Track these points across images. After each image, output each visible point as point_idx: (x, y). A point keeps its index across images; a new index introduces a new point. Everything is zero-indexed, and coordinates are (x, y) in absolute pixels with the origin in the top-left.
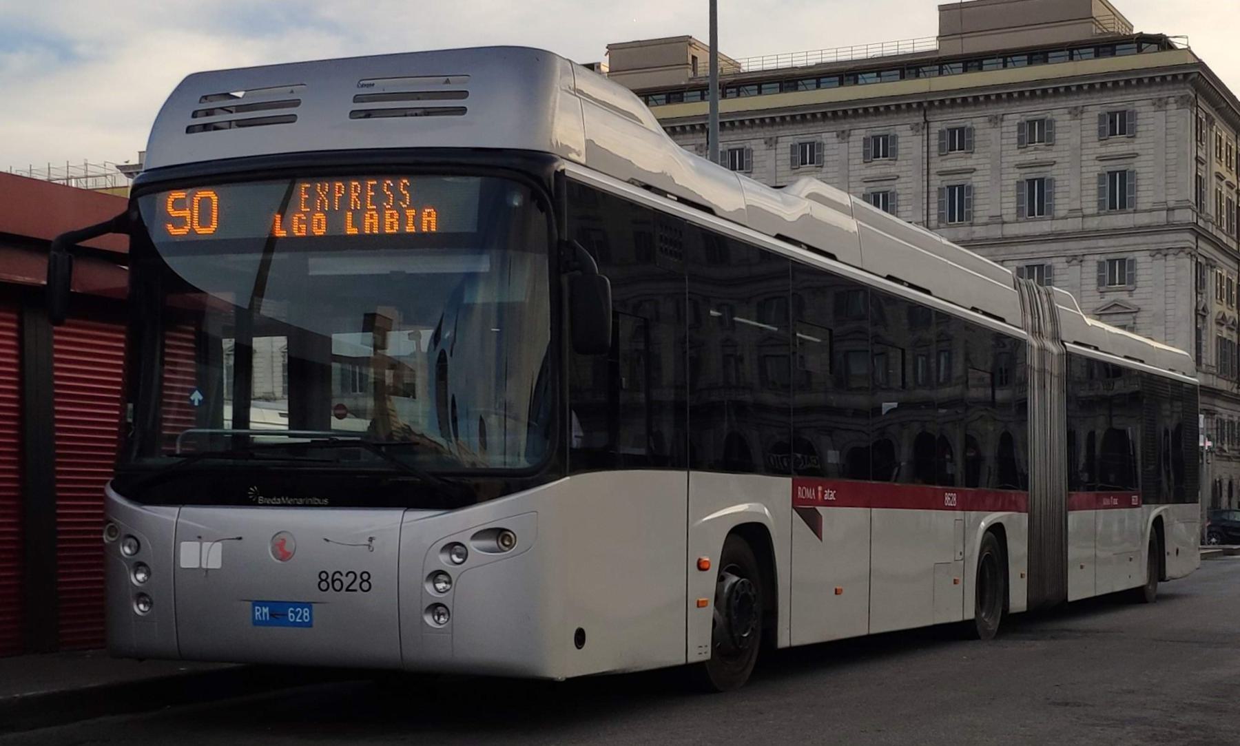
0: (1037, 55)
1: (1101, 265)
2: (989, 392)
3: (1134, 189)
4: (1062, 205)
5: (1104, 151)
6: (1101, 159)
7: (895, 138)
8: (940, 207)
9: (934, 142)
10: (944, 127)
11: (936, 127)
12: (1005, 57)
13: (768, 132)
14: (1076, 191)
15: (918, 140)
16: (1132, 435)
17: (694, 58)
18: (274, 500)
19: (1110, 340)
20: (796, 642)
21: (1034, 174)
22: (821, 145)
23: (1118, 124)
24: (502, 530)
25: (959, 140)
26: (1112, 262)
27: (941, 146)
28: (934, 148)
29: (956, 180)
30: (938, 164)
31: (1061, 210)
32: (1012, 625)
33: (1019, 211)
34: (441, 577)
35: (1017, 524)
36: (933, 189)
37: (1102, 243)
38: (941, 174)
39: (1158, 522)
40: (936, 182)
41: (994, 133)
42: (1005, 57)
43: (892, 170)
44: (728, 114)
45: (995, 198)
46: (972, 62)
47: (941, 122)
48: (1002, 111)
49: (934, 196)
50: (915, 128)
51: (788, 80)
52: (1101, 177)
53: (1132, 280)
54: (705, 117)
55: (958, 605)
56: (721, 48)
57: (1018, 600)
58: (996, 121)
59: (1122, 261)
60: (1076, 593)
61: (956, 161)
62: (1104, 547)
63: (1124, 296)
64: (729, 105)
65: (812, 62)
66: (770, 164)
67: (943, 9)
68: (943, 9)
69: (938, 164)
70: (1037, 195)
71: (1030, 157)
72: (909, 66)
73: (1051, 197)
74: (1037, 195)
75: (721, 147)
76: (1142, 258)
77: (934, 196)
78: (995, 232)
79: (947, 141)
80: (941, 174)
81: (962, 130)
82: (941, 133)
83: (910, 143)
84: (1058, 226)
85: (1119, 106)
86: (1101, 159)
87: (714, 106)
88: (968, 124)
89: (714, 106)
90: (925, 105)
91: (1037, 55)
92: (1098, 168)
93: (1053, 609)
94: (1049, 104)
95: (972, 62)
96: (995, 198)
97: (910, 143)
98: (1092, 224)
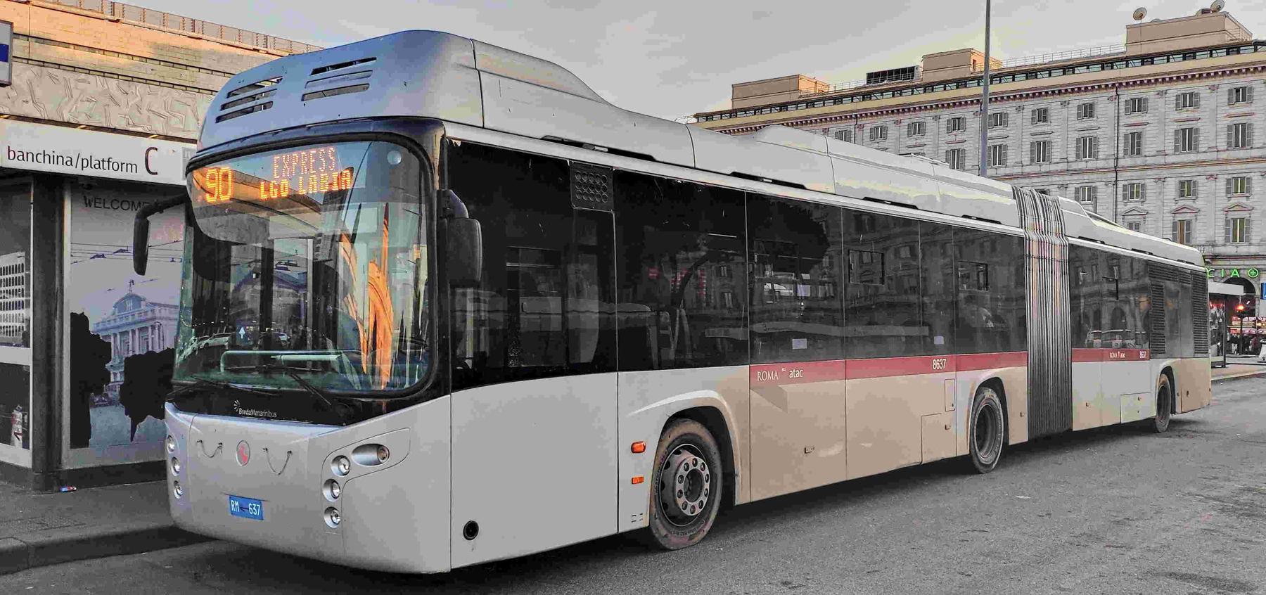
0: (1189, 54)
1: (1228, 181)
2: (570, 307)
3: (1251, 135)
4: (1056, 154)
5: (1232, 111)
9: (1122, 108)
11: (1122, 100)
12: (1168, 55)
14: (1213, 134)
15: (1111, 108)
16: (1136, 302)
18: (247, 412)
19: (1117, 238)
22: (1251, 89)
23: (1042, 116)
25: (1138, 105)
26: (1236, 179)
31: (1010, 161)
32: (1012, 454)
34: (343, 460)
35: (1015, 376)
36: (1121, 135)
37: (1229, 167)
39: (1167, 371)
40: (1123, 131)
41: (1161, 101)
44: (994, 94)
45: (1018, 155)
46: (1147, 59)
47: (1127, 94)
49: (1122, 139)
50: (1110, 99)
53: (1195, 193)
54: (980, 95)
55: (957, 444)
56: (991, 54)
57: (1019, 433)
58: (1020, 109)
59: (1243, 179)
60: (1082, 421)
61: (1136, 118)
62: (1109, 387)
63: (1244, 200)
64: (995, 88)
66: (1019, 121)
68: (733, 86)
69: (1124, 120)
70: (1041, 150)
71: (1184, 115)
72: (1107, 63)
74: (1041, 150)
75: (989, 112)
76: (1201, 180)
77: (1122, 139)
79: (1181, 101)
81: (1140, 100)
83: (1104, 105)
84: (1201, 157)
85: (879, 124)
87: (986, 90)
88: (1144, 96)
89: (986, 90)
90: (1117, 85)
91: (1189, 54)
92: (1176, 126)
93: (1056, 436)
94: (922, 114)
95: (1147, 59)
96: (1018, 155)
98: (1223, 156)
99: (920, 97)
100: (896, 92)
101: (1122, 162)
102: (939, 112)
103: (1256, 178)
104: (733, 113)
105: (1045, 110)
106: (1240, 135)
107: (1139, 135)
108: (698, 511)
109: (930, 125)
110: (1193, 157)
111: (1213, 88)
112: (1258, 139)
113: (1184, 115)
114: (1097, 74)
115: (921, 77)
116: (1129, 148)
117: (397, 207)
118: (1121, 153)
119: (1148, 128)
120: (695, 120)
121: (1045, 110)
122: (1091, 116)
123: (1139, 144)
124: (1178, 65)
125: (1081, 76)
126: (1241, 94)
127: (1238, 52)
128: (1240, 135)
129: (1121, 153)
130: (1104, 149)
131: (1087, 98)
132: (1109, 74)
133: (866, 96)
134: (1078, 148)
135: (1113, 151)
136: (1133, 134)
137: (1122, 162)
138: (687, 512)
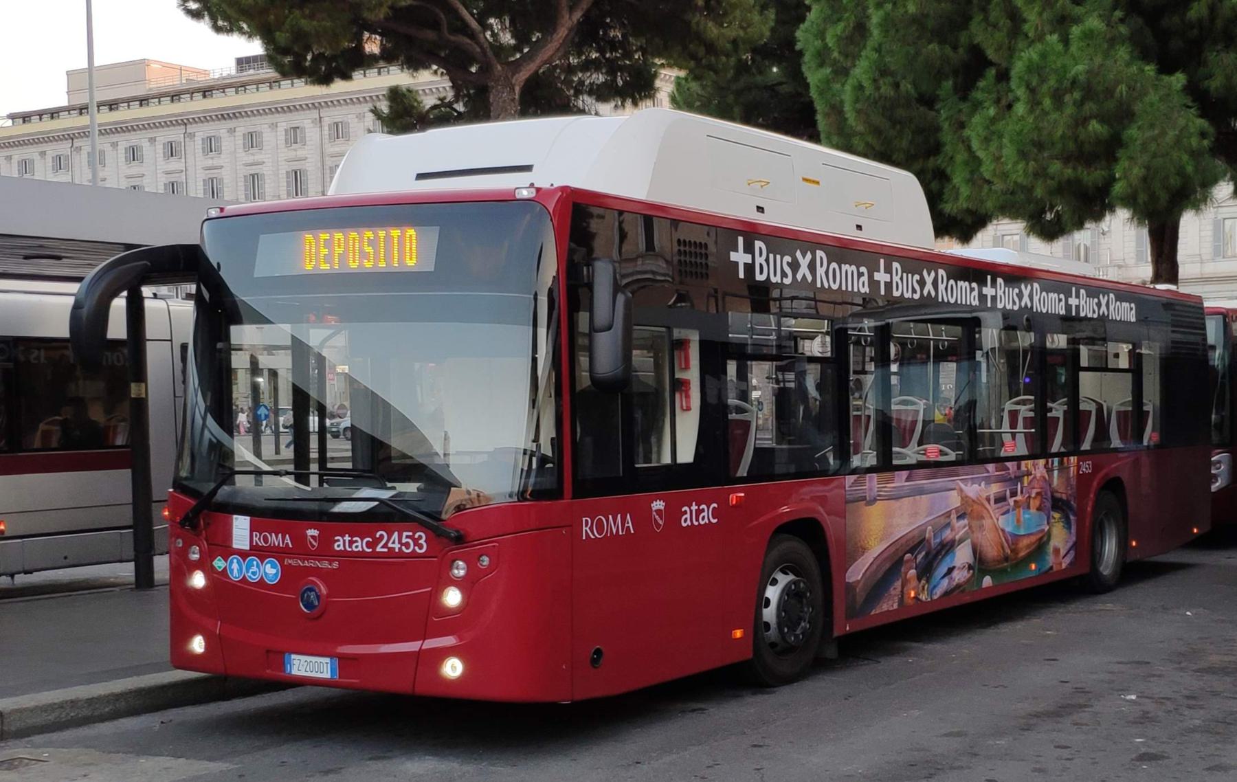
9: (326, 132)
11: (240, 132)
67: (69, 73)
68: (69, 73)
94: (257, 120)
109: (268, 136)
120: (10, 122)
133: (240, 87)
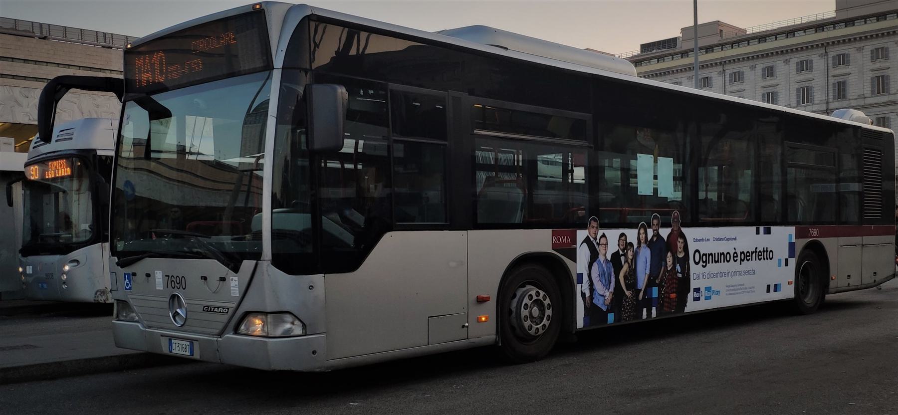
6: (872, 71)
7: (811, 61)
8: (834, 92)
9: (830, 61)
10: (835, 54)
11: (728, 72)
12: (865, 18)
13: (751, 63)
17: (721, 31)
20: (36, 117)
21: (878, 74)
23: (769, 72)
24: (766, 251)
25: (842, 60)
27: (834, 64)
28: (830, 65)
29: (841, 79)
30: (833, 72)
33: (873, 92)
36: (830, 84)
38: (834, 76)
39: (622, 235)
40: (832, 80)
42: (865, 18)
43: (887, 65)
46: (849, 22)
47: (833, 52)
48: (862, 45)
49: (831, 87)
50: (719, 73)
51: (761, 37)
52: (872, 79)
58: (860, 49)
65: (775, 27)
69: (833, 72)
71: (877, 65)
72: (819, 26)
73: (888, 84)
78: (861, 102)
79: (837, 61)
80: (834, 76)
81: (843, 55)
82: (834, 57)
83: (818, 62)
84: (891, 98)
86: (763, 87)
88: (847, 52)
91: (881, 16)
94: (886, 40)
95: (849, 22)
97: (818, 62)
99: (679, 62)
100: (660, 58)
101: (832, 106)
102: (862, 44)
103: (892, 116)
104: (833, 23)
105: (772, 68)
106: (881, 84)
107: (844, 83)
108: (541, 332)
110: (885, 98)
111: (753, 68)
112: (893, 88)
113: (877, 65)
114: (812, 36)
115: (682, 46)
116: (837, 94)
117: (650, 192)
118: (831, 99)
119: (850, 77)
121: (772, 68)
122: (772, 75)
123: (844, 90)
124: (873, 26)
125: (800, 39)
126: (805, 66)
127: (713, 51)
128: (881, 84)
129: (831, 97)
130: (819, 96)
131: (767, 62)
132: (821, 35)
134: (798, 96)
135: (824, 98)
136: (839, 83)
137: (832, 106)
138: (532, 332)
